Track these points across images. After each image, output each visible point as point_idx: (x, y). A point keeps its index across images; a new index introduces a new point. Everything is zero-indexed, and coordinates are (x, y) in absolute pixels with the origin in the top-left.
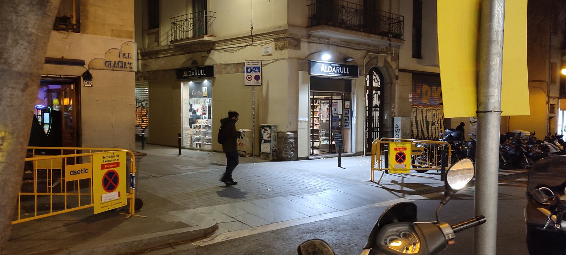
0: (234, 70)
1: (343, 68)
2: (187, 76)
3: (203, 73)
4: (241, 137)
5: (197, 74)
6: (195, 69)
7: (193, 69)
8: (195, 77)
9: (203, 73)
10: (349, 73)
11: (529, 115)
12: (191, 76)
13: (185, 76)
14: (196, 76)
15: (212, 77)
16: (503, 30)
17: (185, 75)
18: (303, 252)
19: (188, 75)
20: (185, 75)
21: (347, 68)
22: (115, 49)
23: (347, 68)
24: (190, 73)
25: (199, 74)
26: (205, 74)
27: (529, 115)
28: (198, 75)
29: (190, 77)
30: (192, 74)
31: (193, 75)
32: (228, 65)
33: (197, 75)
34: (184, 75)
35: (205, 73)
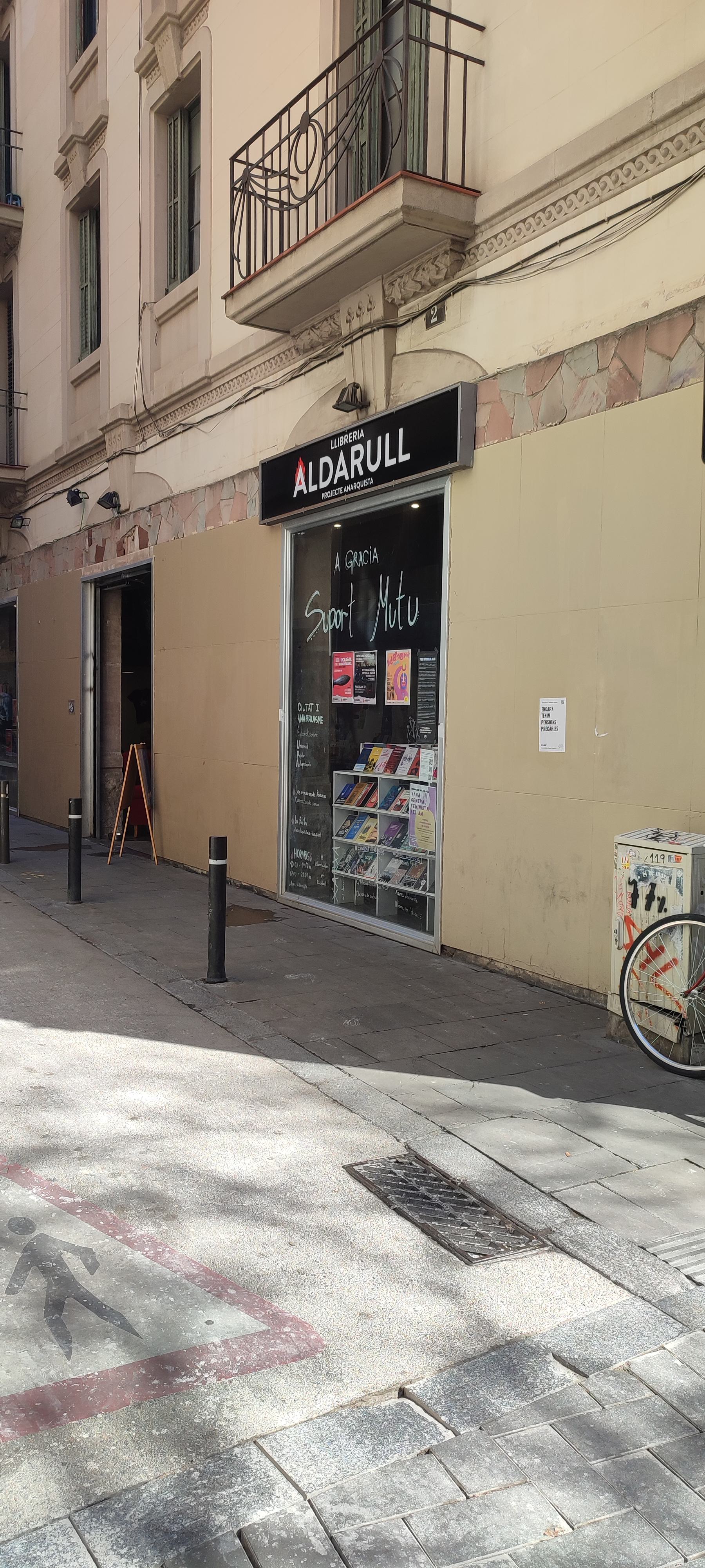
0: (598, 386)
1: (379, 439)
2: (313, 488)
3: (394, 454)
4: (650, 898)
5: (364, 463)
6: (356, 435)
7: (342, 441)
8: (355, 486)
9: (394, 454)
10: (407, 457)
11: (387, 652)
12: (331, 487)
13: (301, 492)
14: (358, 478)
15: (450, 466)
16: (10, 413)
17: (303, 487)
18: (703, 1552)
19: (316, 481)
20: (300, 486)
21: (401, 431)
22: (142, 333)
23: (401, 431)
24: (326, 465)
25: (373, 462)
26: (404, 458)
27: (387, 652)
28: (367, 473)
29: (324, 495)
30: (339, 474)
31: (342, 479)
32: (555, 360)
33: (361, 473)
34: (298, 488)
35: (404, 453)
